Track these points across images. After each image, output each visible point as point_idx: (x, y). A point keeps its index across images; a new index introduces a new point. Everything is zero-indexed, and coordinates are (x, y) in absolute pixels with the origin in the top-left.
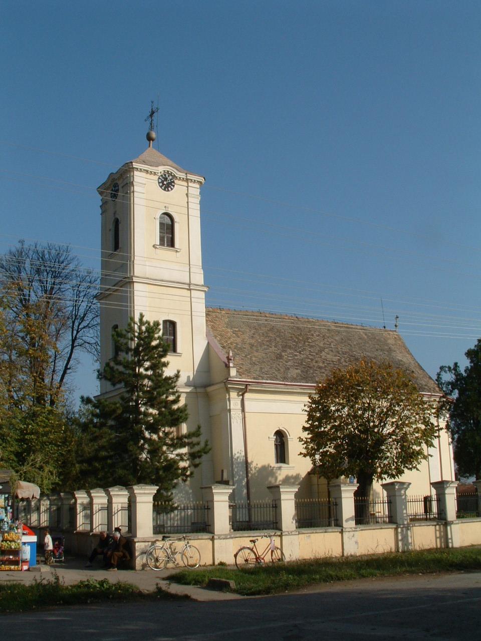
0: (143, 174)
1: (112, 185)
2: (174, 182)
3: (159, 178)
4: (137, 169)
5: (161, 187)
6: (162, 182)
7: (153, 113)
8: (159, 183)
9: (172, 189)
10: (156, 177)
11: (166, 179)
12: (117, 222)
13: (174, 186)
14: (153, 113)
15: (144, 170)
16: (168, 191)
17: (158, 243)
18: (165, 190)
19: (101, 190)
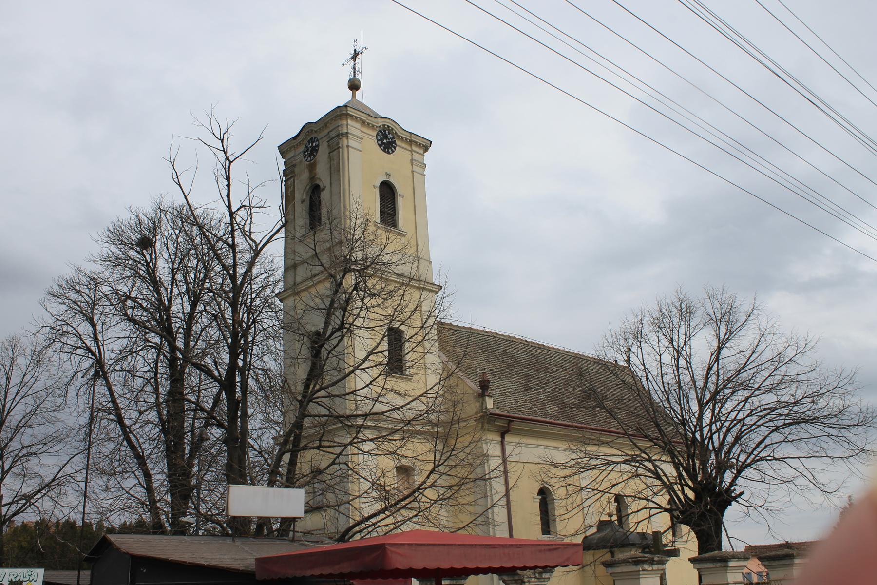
0: (358, 125)
1: (306, 141)
3: (378, 134)
4: (352, 116)
5: (380, 146)
6: (382, 140)
7: (356, 54)
8: (378, 140)
9: (393, 152)
10: (374, 134)
11: (386, 137)
12: (315, 190)
13: (395, 148)
14: (356, 54)
15: (361, 119)
16: (389, 153)
17: (379, 221)
18: (384, 151)
19: (284, 149)
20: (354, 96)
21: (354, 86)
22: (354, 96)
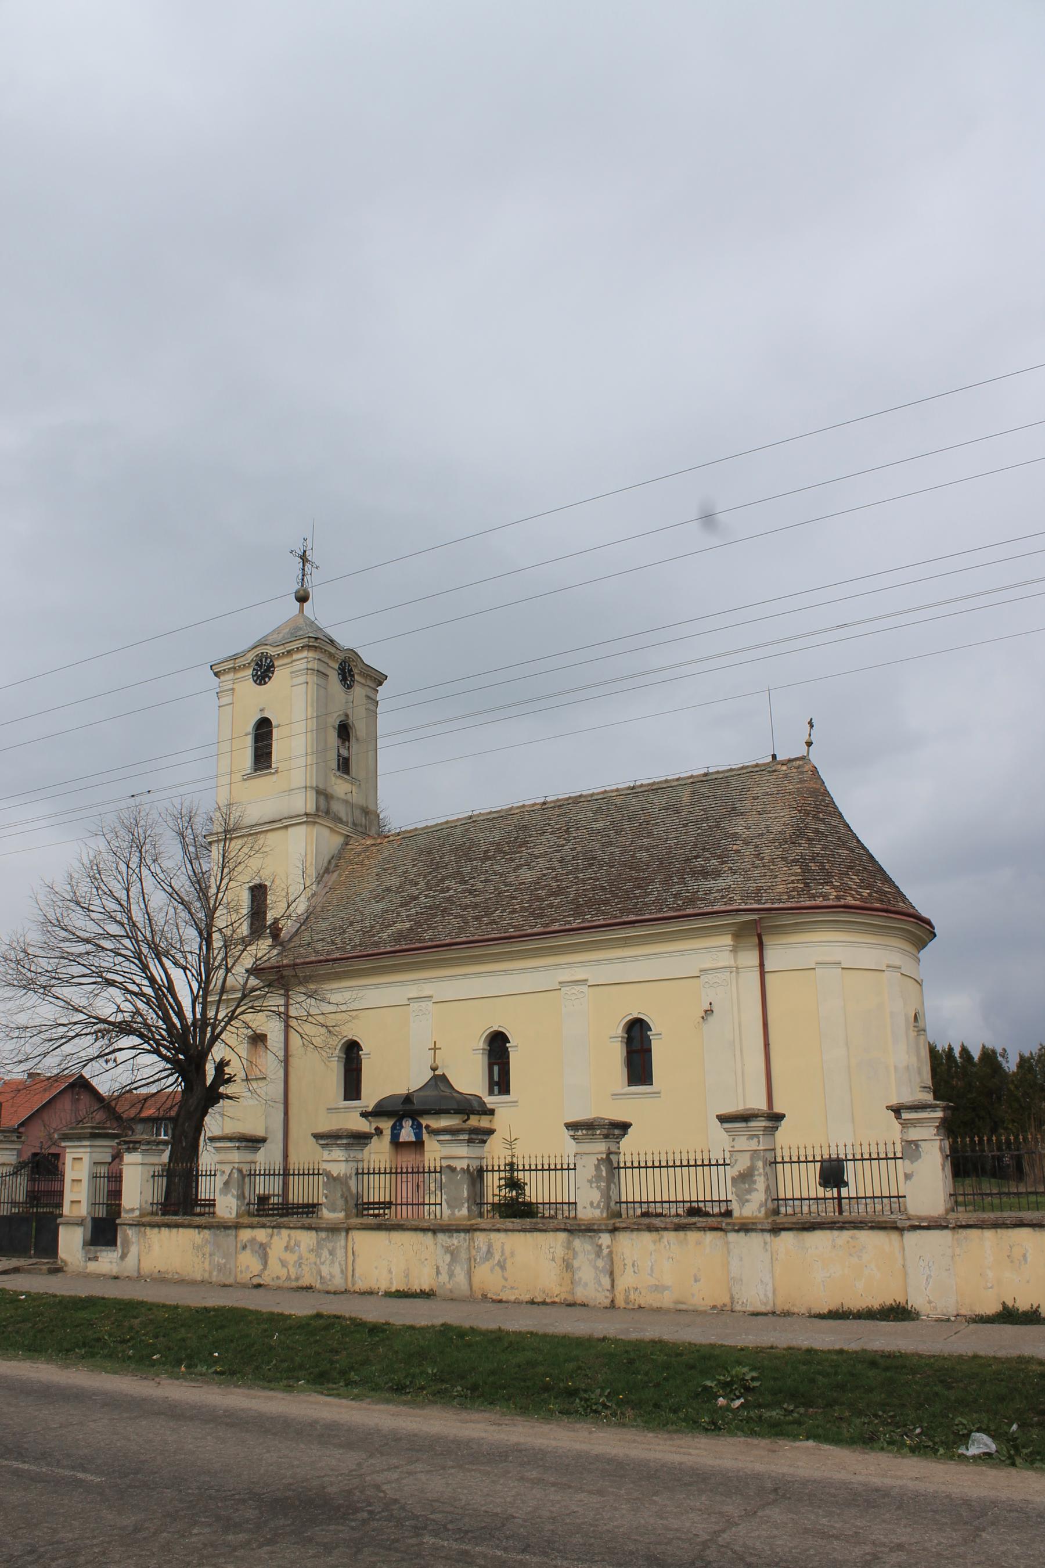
2: (273, 666)
20: (301, 610)
21: (302, 598)
22: (301, 610)
